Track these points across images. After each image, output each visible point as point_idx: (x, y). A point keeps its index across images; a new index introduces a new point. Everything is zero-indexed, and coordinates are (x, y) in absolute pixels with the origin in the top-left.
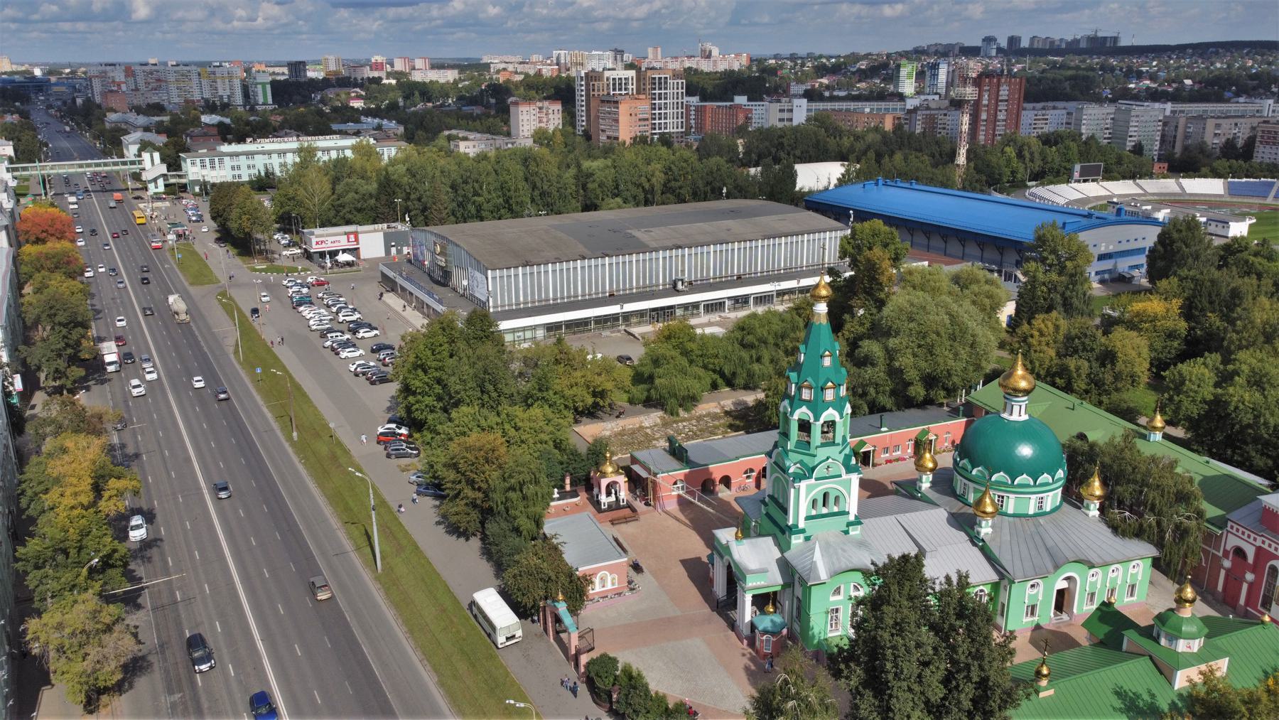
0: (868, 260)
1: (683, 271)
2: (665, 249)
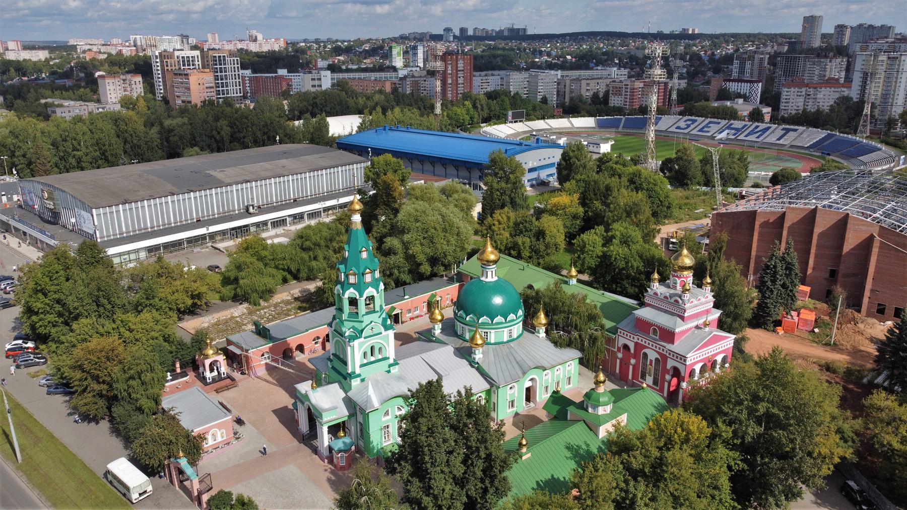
0: (385, 182)
1: (253, 199)
2: (237, 183)
